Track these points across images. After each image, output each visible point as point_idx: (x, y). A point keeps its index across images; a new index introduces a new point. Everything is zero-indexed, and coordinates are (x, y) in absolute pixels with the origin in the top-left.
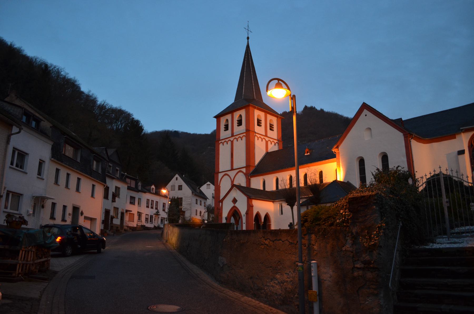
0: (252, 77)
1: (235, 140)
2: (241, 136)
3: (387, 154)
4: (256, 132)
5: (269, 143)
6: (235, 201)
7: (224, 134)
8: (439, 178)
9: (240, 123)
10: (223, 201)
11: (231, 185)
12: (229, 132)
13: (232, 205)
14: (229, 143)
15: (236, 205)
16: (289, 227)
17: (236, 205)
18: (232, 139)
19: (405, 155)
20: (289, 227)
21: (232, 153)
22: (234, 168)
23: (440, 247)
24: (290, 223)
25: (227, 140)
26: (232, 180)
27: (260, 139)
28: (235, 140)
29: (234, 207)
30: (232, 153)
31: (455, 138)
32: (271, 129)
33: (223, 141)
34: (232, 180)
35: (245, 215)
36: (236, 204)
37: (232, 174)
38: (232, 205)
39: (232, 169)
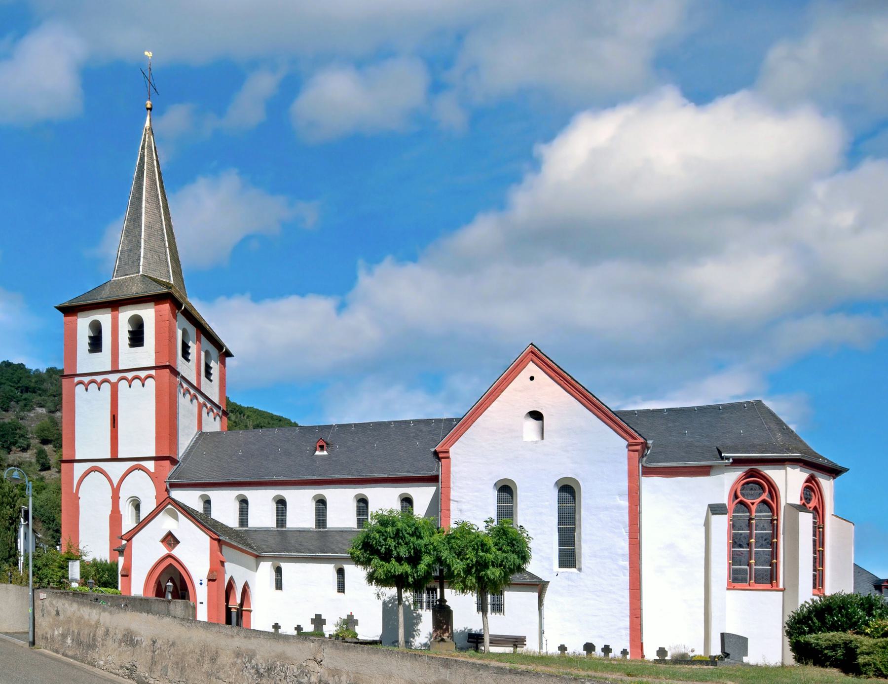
0: (167, 245)
1: (123, 385)
2: (143, 374)
3: (326, 498)
4: (182, 373)
5: (205, 410)
6: (170, 540)
7: (86, 362)
8: (559, 546)
9: (96, 344)
10: (131, 539)
11: (155, 501)
12: (102, 361)
13: (163, 551)
14: (106, 387)
15: (177, 552)
16: (274, 629)
17: (177, 552)
18: (114, 378)
19: (627, 493)
20: (274, 629)
21: (114, 416)
22: (121, 455)
23: (836, 632)
24: (316, 615)
25: (99, 378)
26: (115, 486)
27: (188, 396)
28: (123, 385)
29: (169, 556)
30: (114, 416)
31: (724, 474)
32: (208, 374)
33: (86, 379)
34: (115, 486)
35: (205, 582)
36: (175, 550)
37: (116, 470)
38: (163, 551)
39: (115, 459)
